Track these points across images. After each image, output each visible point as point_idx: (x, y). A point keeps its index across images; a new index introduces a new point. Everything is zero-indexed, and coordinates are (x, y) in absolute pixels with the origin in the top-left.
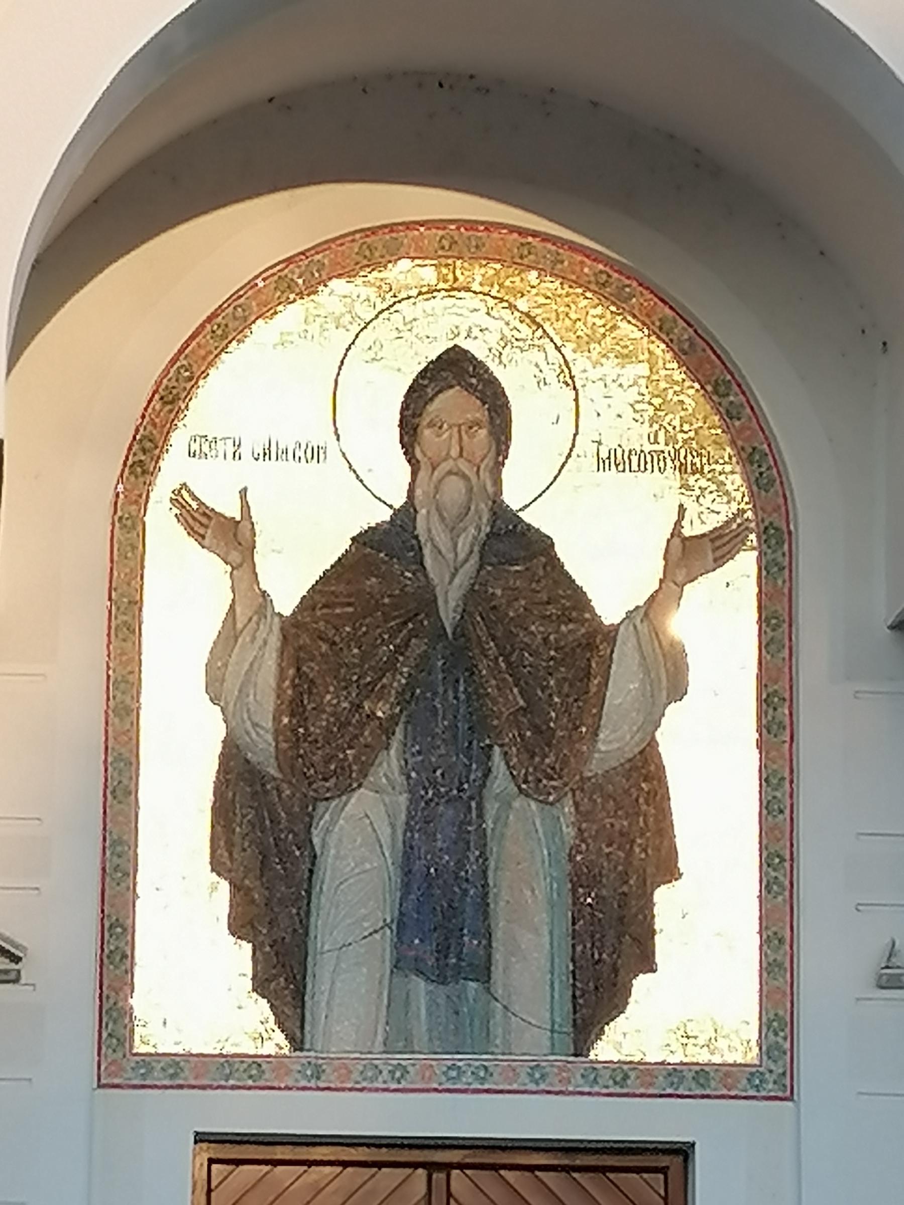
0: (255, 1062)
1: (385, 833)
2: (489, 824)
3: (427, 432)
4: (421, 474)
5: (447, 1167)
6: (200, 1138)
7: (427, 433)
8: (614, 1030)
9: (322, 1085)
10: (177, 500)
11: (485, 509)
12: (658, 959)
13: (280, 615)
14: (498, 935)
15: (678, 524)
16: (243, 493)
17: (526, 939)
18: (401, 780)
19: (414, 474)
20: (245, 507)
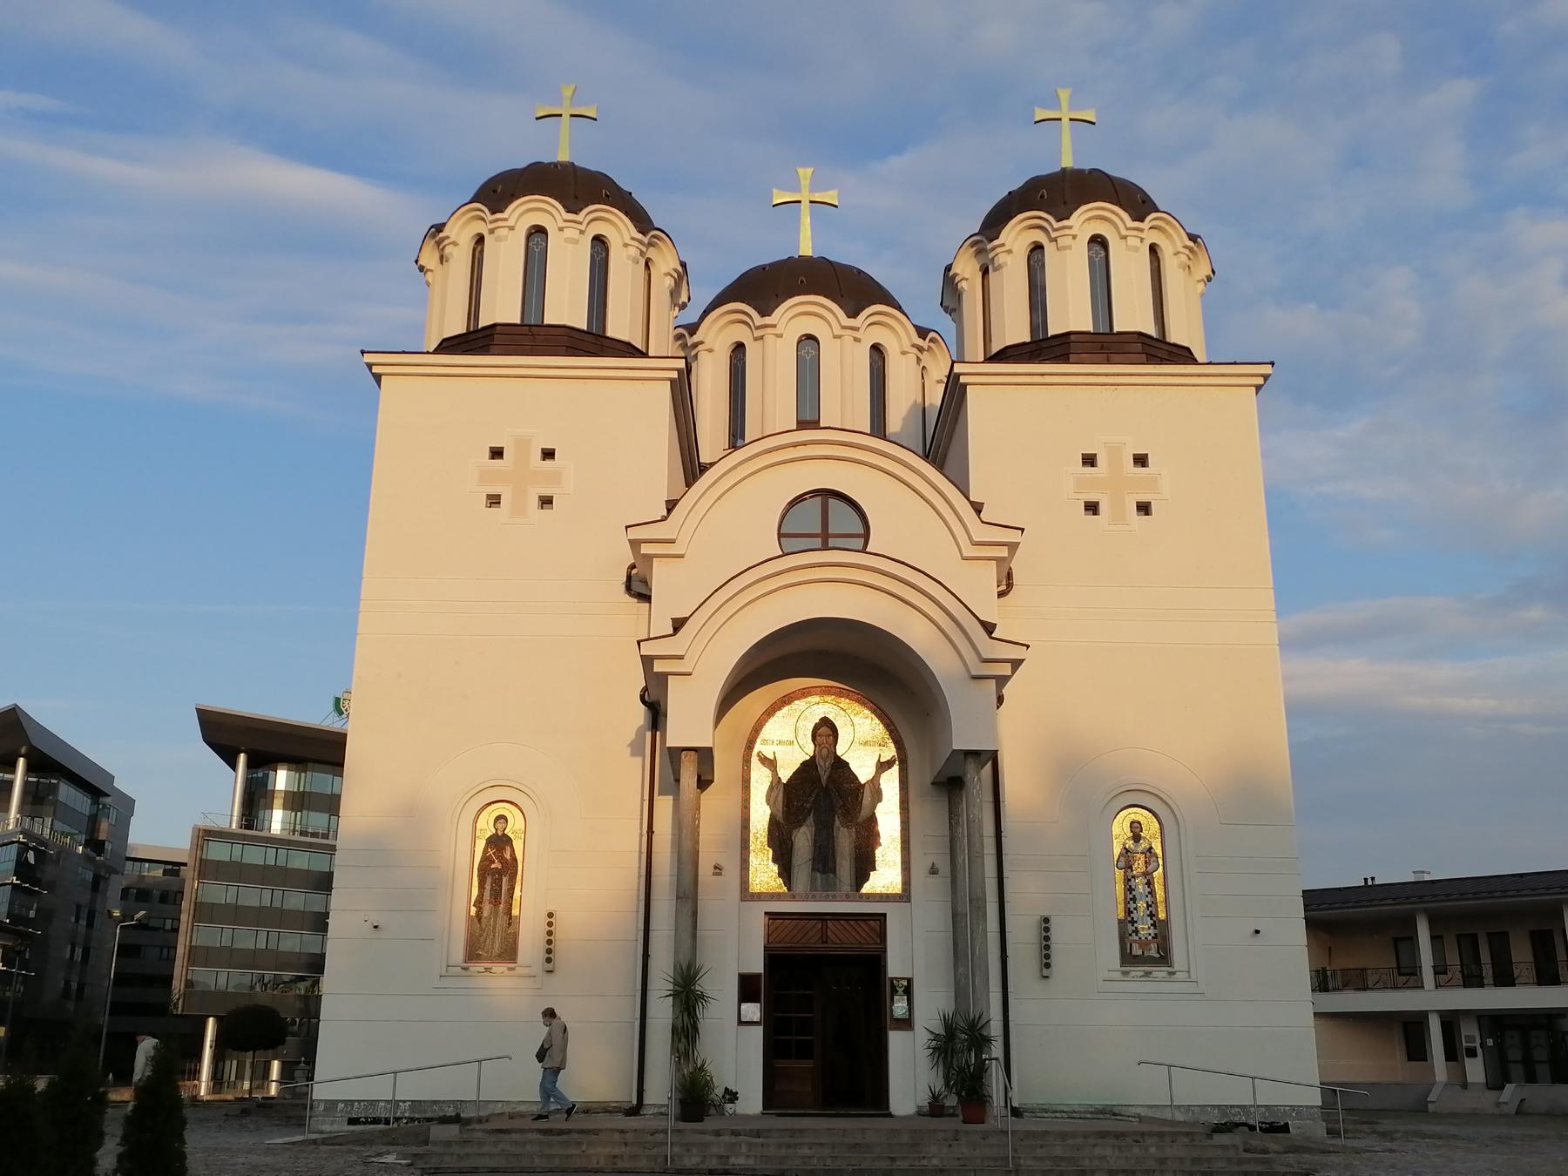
0: (779, 894)
5: (827, 920)
6: (766, 913)
7: (818, 738)
11: (833, 755)
14: (838, 861)
15: (879, 760)
17: (844, 862)
18: (813, 823)
20: (775, 757)
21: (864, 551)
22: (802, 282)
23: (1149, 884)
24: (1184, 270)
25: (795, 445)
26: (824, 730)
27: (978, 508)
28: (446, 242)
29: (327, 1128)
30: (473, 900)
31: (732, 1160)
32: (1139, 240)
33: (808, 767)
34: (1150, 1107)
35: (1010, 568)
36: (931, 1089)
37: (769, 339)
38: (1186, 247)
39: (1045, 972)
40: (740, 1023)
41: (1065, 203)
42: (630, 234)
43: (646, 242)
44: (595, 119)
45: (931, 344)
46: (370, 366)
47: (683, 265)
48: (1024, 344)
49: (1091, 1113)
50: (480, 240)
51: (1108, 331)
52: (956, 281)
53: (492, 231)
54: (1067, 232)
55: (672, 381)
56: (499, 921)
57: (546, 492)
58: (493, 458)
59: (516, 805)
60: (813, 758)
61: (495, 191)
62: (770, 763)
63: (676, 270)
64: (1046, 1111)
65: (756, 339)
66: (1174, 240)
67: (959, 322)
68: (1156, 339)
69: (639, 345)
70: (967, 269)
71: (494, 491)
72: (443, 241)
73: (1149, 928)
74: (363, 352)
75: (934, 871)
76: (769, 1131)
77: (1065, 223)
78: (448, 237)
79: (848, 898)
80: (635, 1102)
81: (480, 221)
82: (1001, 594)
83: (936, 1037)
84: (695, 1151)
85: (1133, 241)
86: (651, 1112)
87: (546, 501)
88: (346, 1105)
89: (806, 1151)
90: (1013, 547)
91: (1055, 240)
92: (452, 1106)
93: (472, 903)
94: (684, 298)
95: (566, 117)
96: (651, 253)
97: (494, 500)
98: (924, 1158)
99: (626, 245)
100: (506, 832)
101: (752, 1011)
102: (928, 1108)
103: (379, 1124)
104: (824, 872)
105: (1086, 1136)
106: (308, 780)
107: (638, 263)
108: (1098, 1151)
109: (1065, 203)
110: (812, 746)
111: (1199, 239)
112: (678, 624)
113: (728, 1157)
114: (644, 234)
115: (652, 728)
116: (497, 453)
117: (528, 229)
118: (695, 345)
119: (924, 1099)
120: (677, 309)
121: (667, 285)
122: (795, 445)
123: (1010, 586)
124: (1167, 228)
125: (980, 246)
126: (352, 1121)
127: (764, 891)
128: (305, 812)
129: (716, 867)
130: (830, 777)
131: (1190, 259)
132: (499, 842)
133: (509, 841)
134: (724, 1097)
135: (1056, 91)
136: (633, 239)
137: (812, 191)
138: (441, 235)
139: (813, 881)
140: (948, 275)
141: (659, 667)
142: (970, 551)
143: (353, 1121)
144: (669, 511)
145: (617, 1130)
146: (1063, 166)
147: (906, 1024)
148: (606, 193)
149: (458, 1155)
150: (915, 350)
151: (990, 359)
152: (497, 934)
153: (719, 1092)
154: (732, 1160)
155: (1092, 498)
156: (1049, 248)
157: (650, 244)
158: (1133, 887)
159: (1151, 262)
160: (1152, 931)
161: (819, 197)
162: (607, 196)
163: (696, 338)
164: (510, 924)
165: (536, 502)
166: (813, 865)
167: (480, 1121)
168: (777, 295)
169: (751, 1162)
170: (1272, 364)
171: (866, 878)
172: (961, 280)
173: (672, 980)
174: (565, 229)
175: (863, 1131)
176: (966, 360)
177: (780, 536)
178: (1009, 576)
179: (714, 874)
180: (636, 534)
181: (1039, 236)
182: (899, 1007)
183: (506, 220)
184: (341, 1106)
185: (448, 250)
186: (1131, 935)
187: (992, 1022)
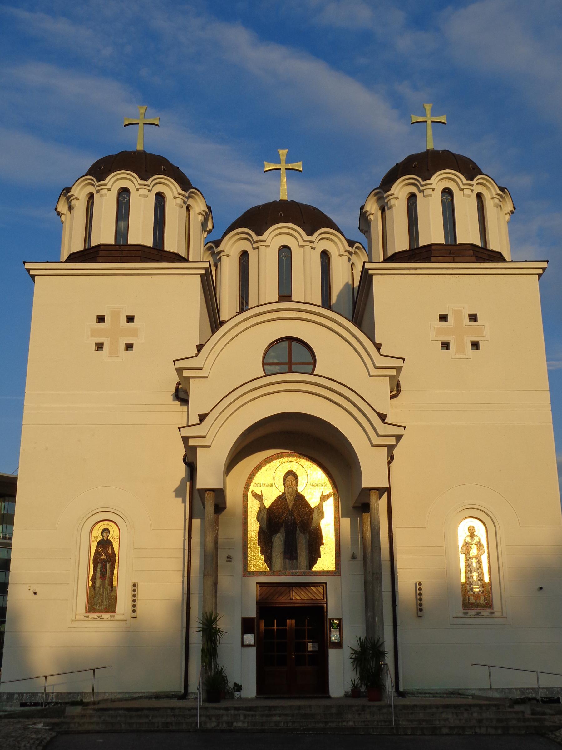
1: (282, 539)
2: (297, 537)
3: (287, 482)
4: (286, 488)
8: (315, 566)
9: (274, 575)
10: (252, 493)
12: (321, 556)
13: (267, 508)
16: (261, 491)
19: (285, 487)
21: (312, 374)
22: (281, 215)
23: (479, 562)
24: (497, 208)
25: (272, 311)
26: (290, 478)
27: (378, 347)
28: (72, 198)
29: (8, 708)
30: (90, 577)
31: (235, 724)
32: (471, 191)
33: (281, 499)
34: (480, 690)
35: (399, 381)
36: (352, 681)
37: (262, 249)
38: (498, 194)
39: (420, 614)
40: (243, 646)
41: (428, 170)
42: (177, 191)
43: (187, 196)
44: (158, 125)
45: (357, 250)
46: (28, 270)
47: (209, 208)
48: (406, 251)
49: (446, 694)
50: (91, 196)
51: (454, 243)
52: (367, 215)
53: (98, 192)
54: (429, 186)
55: (202, 275)
56: (105, 590)
57: (129, 341)
58: (99, 322)
59: (114, 523)
60: (284, 494)
61: (100, 168)
62: (259, 497)
63: (204, 211)
64: (421, 693)
65: (254, 249)
66: (491, 190)
67: (369, 238)
68: (481, 248)
69: (182, 254)
70: (372, 207)
71: (99, 341)
72: (71, 197)
73: (479, 587)
74: (24, 263)
75: (354, 557)
76: (257, 707)
77: (428, 181)
78: (73, 195)
79: (305, 574)
80: (183, 691)
81: (91, 186)
82: (392, 397)
83: (356, 652)
84: (214, 719)
85: (467, 192)
86: (192, 697)
87: (129, 346)
88: (19, 695)
89: (277, 719)
90: (399, 369)
91: (422, 191)
92: (80, 695)
93: (90, 579)
94: (210, 227)
95: (141, 124)
96: (190, 202)
97: (100, 346)
98: (344, 721)
99: (175, 198)
100: (109, 538)
101: (250, 639)
102: (351, 692)
103: (38, 706)
104: (290, 559)
105: (437, 707)
106: (6, 507)
107: (182, 208)
108: (444, 716)
109: (428, 170)
110: (283, 487)
111: (506, 190)
112: (202, 418)
113: (232, 723)
114: (186, 191)
115: (190, 480)
116: (101, 319)
117: (119, 189)
118: (219, 253)
119: (348, 688)
120: (206, 234)
121: (199, 220)
122: (272, 311)
123: (399, 391)
124: (487, 184)
125: (379, 195)
126: (23, 705)
127: (256, 570)
128: (5, 525)
129: (228, 558)
130: (294, 505)
131: (500, 201)
132: (105, 544)
133: (110, 543)
134: (234, 688)
135: (423, 105)
136: (179, 194)
137: (288, 162)
138: (69, 194)
139: (284, 564)
140: (362, 212)
141: (191, 443)
142: (373, 372)
143: (23, 705)
144: (199, 351)
145: (169, 708)
146: (428, 148)
147: (338, 645)
148: (163, 168)
149: (79, 723)
150: (347, 254)
151: (386, 260)
152: (104, 596)
153: (231, 685)
154: (235, 724)
155: (445, 339)
156: (419, 196)
157: (189, 197)
158: (470, 564)
159: (478, 203)
160: (481, 589)
161: (291, 166)
162: (164, 170)
163: (220, 249)
164: (111, 591)
165: (123, 346)
166: (284, 555)
167: (94, 703)
168: (266, 223)
169: (246, 725)
170: (547, 261)
171: (315, 562)
172: (370, 215)
173: (202, 622)
174: (140, 190)
175: (310, 706)
176: (373, 261)
177: (264, 364)
178: (398, 385)
179: (227, 561)
180: (180, 365)
181: (413, 189)
182: (334, 636)
183: (106, 185)
184: (16, 696)
185: (74, 202)
186: (469, 591)
187: (385, 642)
